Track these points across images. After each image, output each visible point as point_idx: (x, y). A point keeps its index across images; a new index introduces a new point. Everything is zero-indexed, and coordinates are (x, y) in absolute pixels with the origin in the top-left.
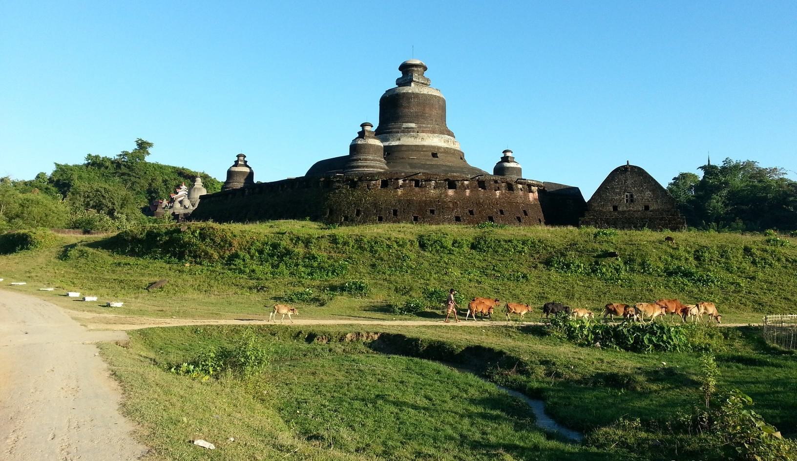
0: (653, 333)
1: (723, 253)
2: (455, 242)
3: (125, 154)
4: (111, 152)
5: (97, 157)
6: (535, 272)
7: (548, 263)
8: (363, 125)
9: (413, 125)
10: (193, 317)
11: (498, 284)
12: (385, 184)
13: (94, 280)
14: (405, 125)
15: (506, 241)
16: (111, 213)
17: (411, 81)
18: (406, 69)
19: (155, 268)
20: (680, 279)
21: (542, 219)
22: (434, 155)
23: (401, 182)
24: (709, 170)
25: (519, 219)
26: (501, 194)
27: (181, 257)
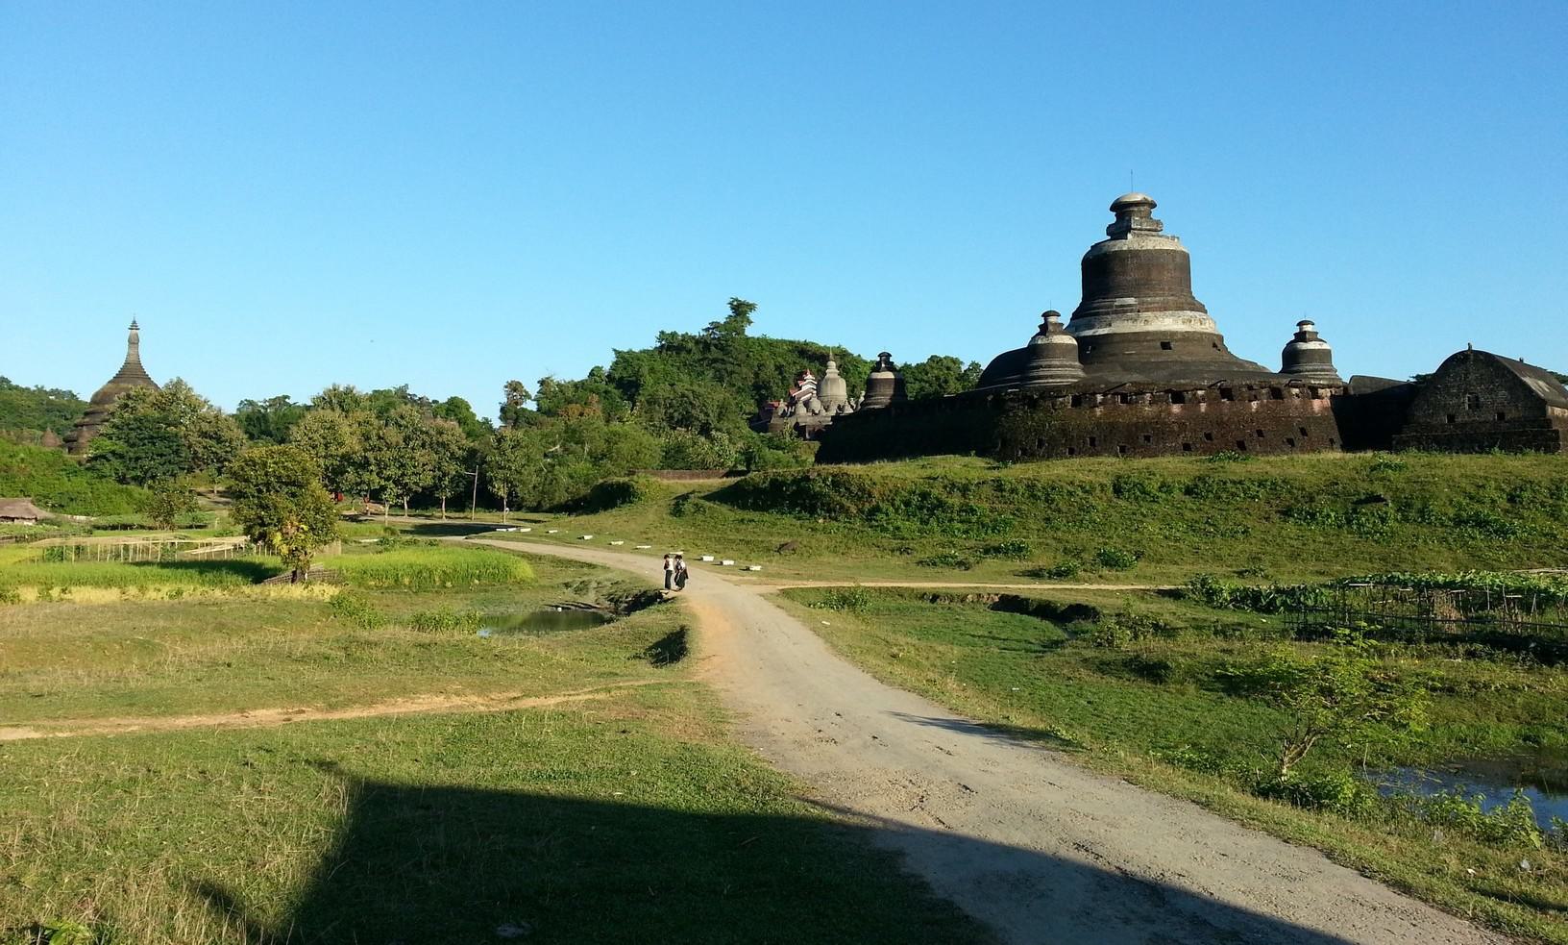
3: (715, 326)
4: (693, 324)
5: (674, 334)
8: (1046, 315)
9: (1131, 301)
10: (827, 580)
12: (1077, 402)
13: (718, 541)
14: (1119, 302)
15: (1234, 482)
16: (705, 430)
17: (1129, 229)
18: (1121, 209)
19: (784, 525)
21: (1336, 436)
22: (1165, 346)
23: (1099, 397)
25: (1291, 442)
26: (1261, 405)
27: (812, 511)
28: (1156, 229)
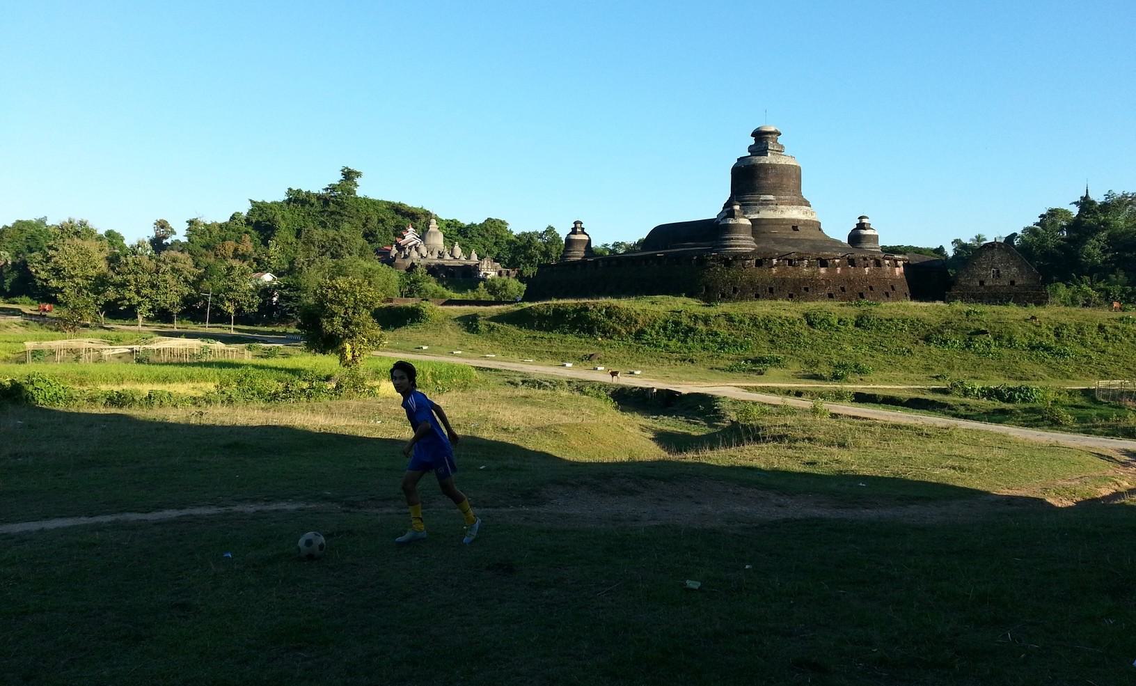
0: (1021, 392)
1: (1080, 330)
2: (840, 320)
5: (299, 191)
6: (917, 347)
7: (927, 339)
9: (771, 197)
11: (889, 357)
14: (763, 197)
18: (760, 136)
20: (1041, 353)
21: (907, 290)
22: (795, 228)
23: (775, 261)
24: (1085, 204)
25: (887, 294)
28: (780, 150)
